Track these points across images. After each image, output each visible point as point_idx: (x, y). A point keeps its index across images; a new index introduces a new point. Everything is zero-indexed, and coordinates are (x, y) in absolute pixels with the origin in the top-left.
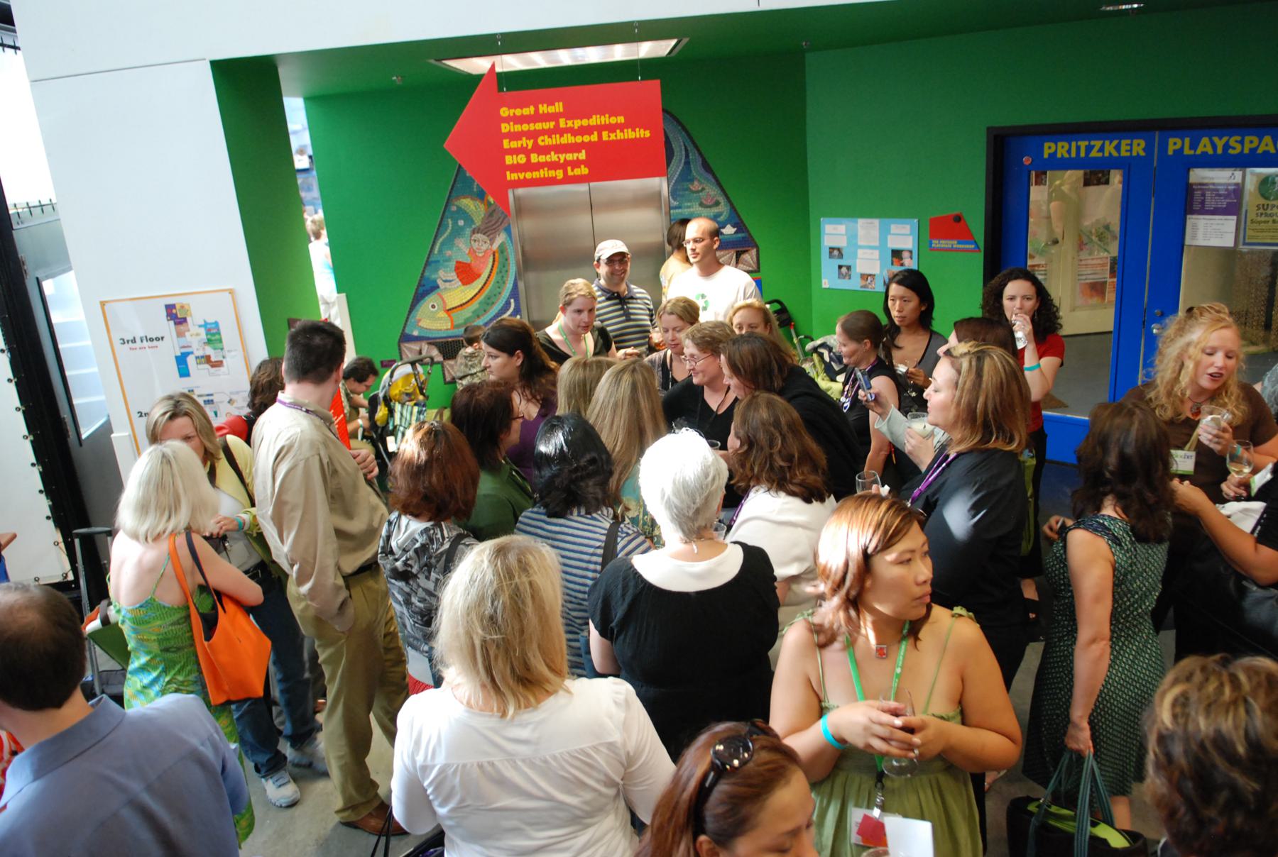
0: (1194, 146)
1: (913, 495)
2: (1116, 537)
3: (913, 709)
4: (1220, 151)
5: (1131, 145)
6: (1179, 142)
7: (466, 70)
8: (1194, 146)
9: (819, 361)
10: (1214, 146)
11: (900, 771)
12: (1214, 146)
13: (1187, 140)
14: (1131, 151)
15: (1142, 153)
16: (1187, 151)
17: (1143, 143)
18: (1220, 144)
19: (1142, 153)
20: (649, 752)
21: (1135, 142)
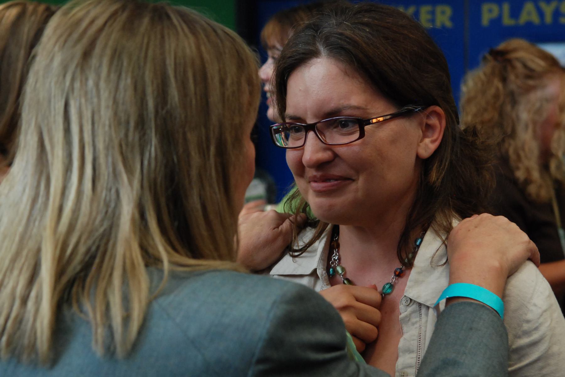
0: (515, 13)
1: (293, 253)
2: (439, 224)
3: (220, 271)
4: (548, 19)
5: (433, 13)
6: (495, 8)
7: (274, 268)
8: (515, 13)
9: (133, 220)
10: (541, 14)
11: (452, 279)
12: (541, 14)
13: (506, 8)
14: (433, 21)
15: (448, 24)
16: (507, 21)
17: (448, 10)
18: (548, 10)
19: (448, 24)
20: (100, 65)
21: (439, 9)
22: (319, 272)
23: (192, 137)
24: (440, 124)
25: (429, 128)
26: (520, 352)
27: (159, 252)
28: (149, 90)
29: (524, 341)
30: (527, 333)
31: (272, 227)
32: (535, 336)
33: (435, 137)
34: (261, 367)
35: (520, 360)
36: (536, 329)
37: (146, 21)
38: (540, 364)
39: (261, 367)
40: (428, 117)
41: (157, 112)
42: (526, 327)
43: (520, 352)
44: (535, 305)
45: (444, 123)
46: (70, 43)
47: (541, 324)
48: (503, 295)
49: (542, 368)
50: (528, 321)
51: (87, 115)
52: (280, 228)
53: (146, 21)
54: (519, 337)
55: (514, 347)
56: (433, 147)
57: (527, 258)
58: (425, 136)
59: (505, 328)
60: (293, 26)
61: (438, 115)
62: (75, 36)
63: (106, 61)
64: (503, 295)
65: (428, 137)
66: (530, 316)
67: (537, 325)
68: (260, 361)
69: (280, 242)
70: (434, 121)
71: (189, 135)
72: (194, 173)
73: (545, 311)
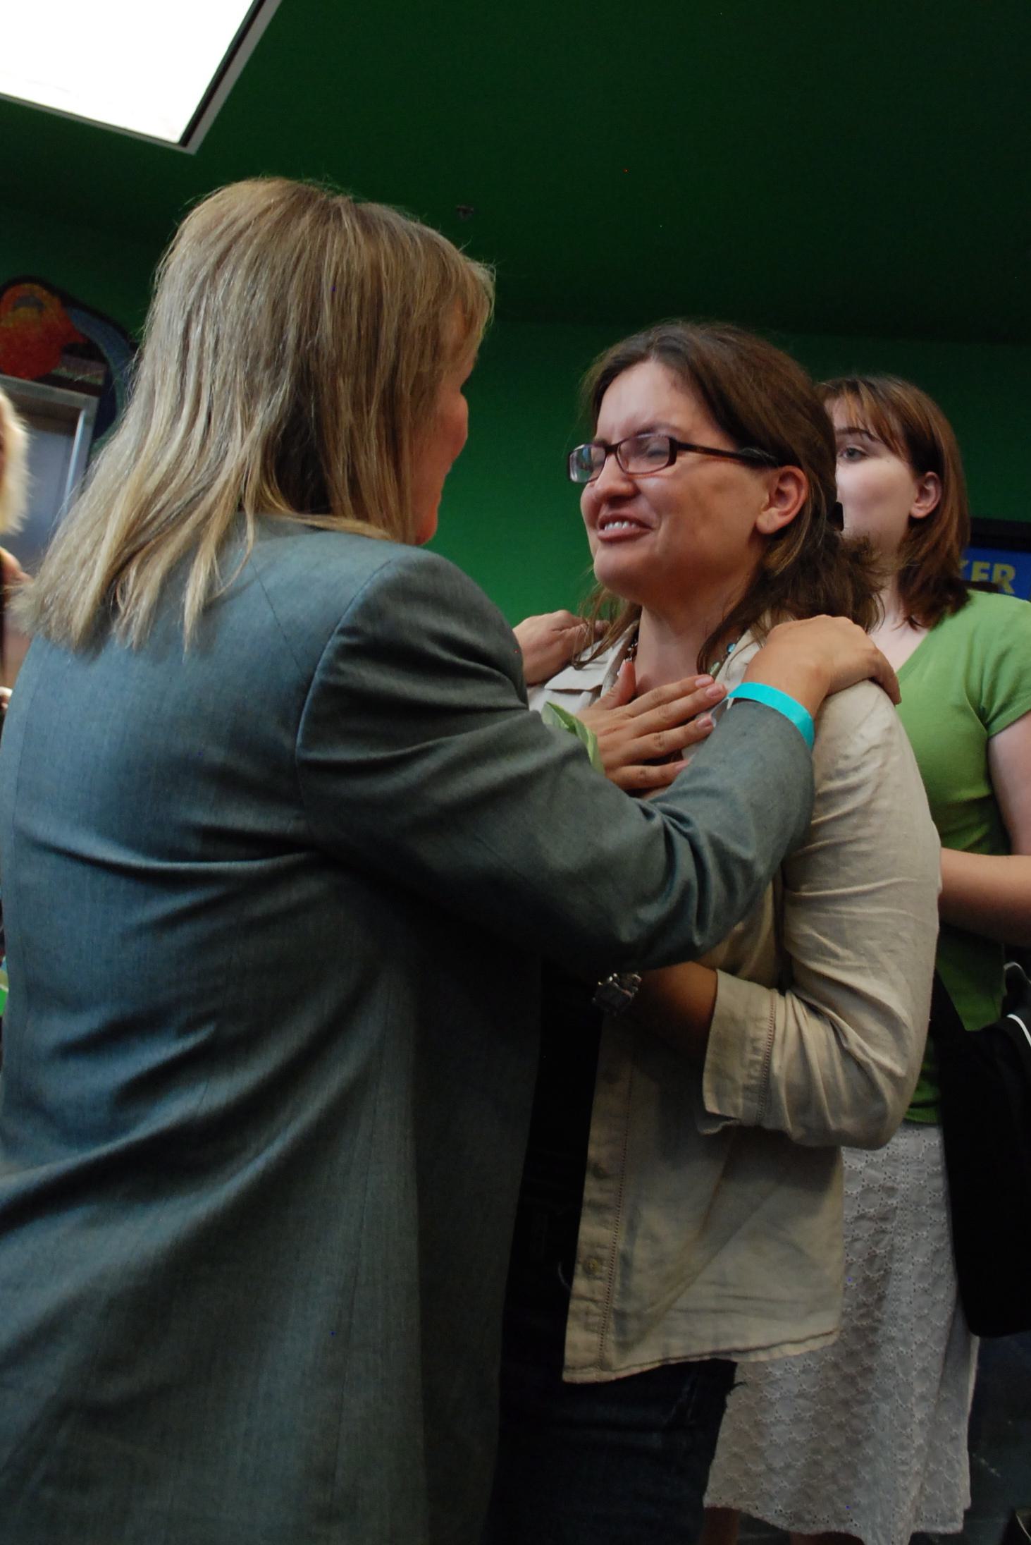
22: (604, 692)
23: (344, 387)
24: (799, 494)
25: (779, 496)
26: (829, 798)
27: (845, 1071)
28: (293, 316)
29: (837, 784)
30: (841, 774)
31: (554, 627)
32: (853, 779)
33: (788, 507)
34: (344, 640)
35: (826, 811)
36: (856, 769)
37: (307, 219)
38: (854, 820)
39: (344, 640)
40: (783, 479)
41: (298, 345)
42: (842, 764)
43: (829, 798)
44: (862, 737)
45: (804, 493)
46: (204, 246)
47: (863, 764)
48: (818, 717)
49: (857, 827)
50: (846, 757)
51: (210, 340)
52: (564, 631)
53: (307, 219)
54: (831, 778)
55: (820, 791)
56: (781, 521)
57: (870, 677)
58: (771, 504)
59: (811, 762)
60: (823, 536)
61: (798, 482)
62: (212, 238)
63: (241, 272)
64: (818, 717)
65: (775, 506)
66: (851, 751)
67: (859, 763)
68: (345, 631)
69: (558, 648)
70: (790, 487)
71: (340, 382)
72: (343, 436)
73: (876, 747)
